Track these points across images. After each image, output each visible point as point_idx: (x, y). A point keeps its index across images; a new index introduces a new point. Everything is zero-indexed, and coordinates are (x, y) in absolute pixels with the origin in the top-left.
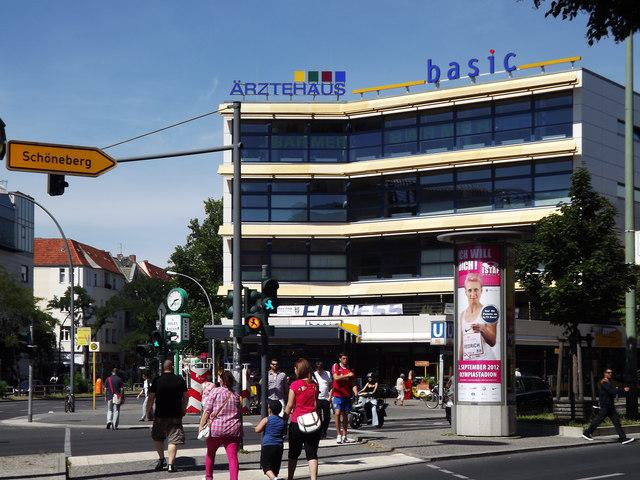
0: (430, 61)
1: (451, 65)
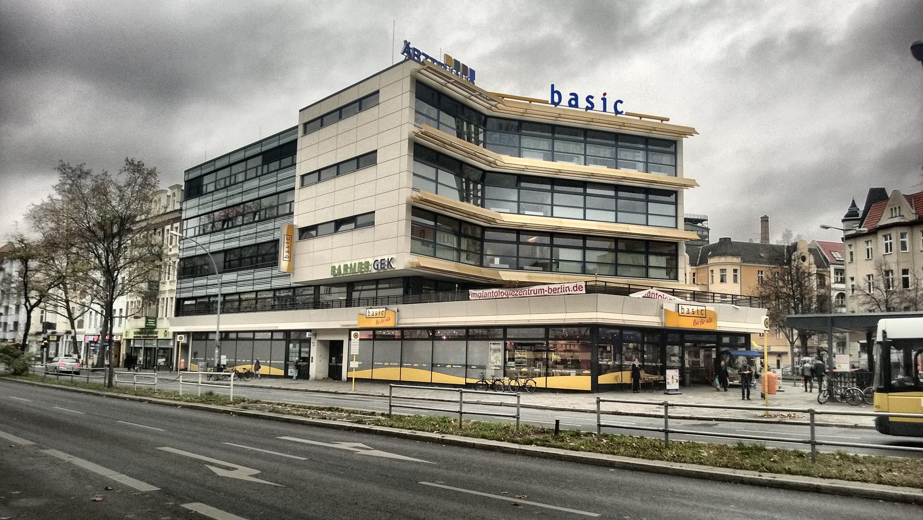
0: (553, 86)
1: (571, 94)
